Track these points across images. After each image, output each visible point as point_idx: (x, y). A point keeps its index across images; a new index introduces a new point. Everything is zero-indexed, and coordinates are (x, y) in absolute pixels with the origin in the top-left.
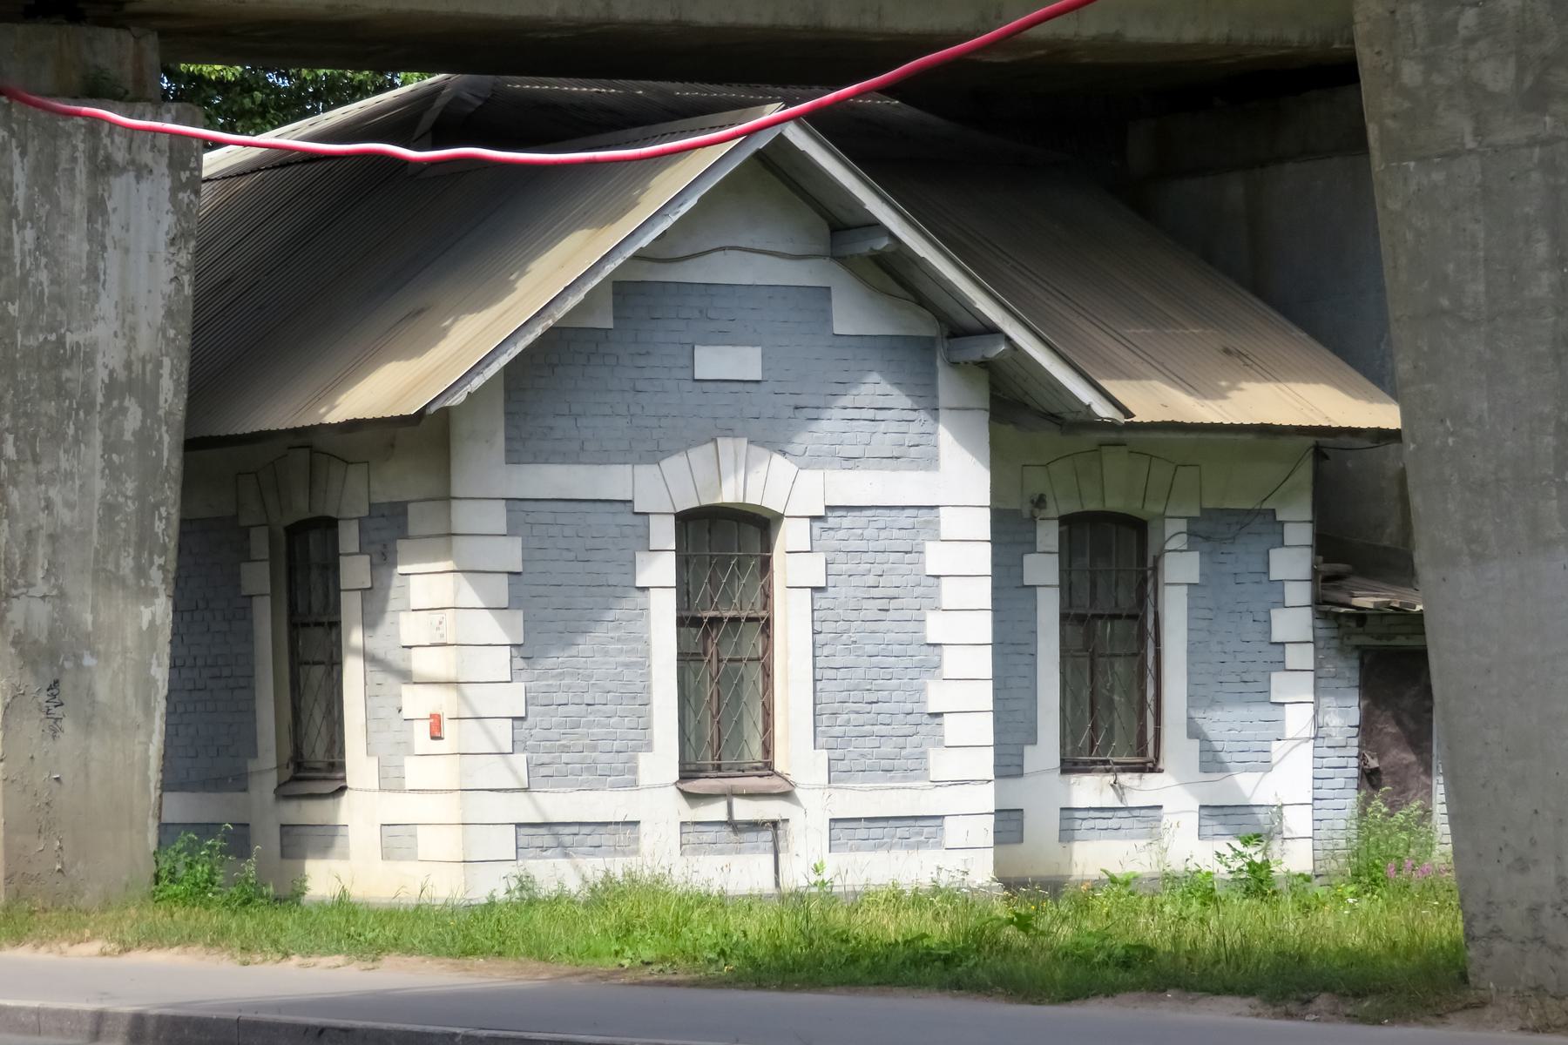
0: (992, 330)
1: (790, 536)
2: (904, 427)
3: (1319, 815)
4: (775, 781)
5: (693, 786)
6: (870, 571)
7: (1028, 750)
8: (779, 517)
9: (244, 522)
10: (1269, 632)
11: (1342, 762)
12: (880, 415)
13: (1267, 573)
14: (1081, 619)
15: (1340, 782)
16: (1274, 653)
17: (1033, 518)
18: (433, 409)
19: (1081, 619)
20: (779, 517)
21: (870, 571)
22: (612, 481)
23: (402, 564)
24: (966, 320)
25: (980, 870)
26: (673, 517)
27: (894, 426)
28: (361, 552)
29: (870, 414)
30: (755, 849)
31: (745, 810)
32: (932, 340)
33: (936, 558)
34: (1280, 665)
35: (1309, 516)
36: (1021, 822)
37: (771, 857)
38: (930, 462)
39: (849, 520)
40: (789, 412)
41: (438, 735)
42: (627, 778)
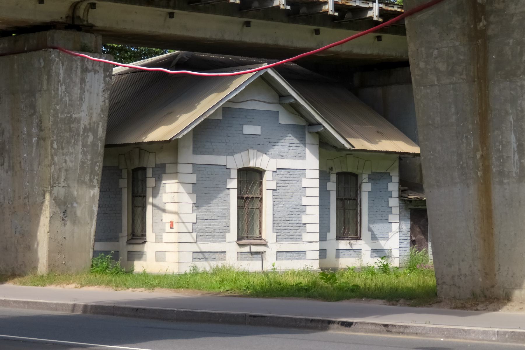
0: (320, 124)
1: (267, 176)
2: (297, 148)
3: (401, 252)
4: (262, 241)
5: (241, 242)
6: (288, 186)
7: (328, 234)
8: (265, 171)
9: (121, 167)
10: (388, 204)
11: (406, 238)
12: (291, 145)
13: (388, 189)
14: (341, 200)
15: (405, 243)
16: (389, 210)
17: (330, 173)
18: (173, 139)
19: (341, 200)
20: (265, 171)
21: (288, 186)
22: (221, 160)
23: (164, 180)
24: (313, 121)
25: (315, 266)
26: (237, 170)
27: (295, 148)
28: (153, 177)
29: (288, 145)
30: (257, 260)
31: (254, 249)
32: (304, 126)
33: (305, 183)
34: (391, 213)
35: (398, 175)
36: (326, 253)
37: (261, 262)
38: (304, 158)
39: (283, 172)
40: (268, 143)
41: (172, 227)
42: (223, 240)
